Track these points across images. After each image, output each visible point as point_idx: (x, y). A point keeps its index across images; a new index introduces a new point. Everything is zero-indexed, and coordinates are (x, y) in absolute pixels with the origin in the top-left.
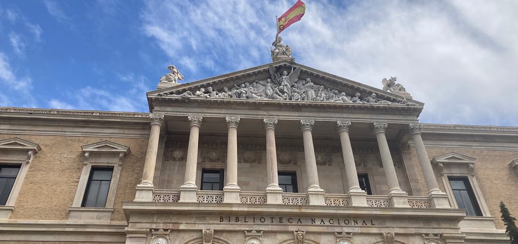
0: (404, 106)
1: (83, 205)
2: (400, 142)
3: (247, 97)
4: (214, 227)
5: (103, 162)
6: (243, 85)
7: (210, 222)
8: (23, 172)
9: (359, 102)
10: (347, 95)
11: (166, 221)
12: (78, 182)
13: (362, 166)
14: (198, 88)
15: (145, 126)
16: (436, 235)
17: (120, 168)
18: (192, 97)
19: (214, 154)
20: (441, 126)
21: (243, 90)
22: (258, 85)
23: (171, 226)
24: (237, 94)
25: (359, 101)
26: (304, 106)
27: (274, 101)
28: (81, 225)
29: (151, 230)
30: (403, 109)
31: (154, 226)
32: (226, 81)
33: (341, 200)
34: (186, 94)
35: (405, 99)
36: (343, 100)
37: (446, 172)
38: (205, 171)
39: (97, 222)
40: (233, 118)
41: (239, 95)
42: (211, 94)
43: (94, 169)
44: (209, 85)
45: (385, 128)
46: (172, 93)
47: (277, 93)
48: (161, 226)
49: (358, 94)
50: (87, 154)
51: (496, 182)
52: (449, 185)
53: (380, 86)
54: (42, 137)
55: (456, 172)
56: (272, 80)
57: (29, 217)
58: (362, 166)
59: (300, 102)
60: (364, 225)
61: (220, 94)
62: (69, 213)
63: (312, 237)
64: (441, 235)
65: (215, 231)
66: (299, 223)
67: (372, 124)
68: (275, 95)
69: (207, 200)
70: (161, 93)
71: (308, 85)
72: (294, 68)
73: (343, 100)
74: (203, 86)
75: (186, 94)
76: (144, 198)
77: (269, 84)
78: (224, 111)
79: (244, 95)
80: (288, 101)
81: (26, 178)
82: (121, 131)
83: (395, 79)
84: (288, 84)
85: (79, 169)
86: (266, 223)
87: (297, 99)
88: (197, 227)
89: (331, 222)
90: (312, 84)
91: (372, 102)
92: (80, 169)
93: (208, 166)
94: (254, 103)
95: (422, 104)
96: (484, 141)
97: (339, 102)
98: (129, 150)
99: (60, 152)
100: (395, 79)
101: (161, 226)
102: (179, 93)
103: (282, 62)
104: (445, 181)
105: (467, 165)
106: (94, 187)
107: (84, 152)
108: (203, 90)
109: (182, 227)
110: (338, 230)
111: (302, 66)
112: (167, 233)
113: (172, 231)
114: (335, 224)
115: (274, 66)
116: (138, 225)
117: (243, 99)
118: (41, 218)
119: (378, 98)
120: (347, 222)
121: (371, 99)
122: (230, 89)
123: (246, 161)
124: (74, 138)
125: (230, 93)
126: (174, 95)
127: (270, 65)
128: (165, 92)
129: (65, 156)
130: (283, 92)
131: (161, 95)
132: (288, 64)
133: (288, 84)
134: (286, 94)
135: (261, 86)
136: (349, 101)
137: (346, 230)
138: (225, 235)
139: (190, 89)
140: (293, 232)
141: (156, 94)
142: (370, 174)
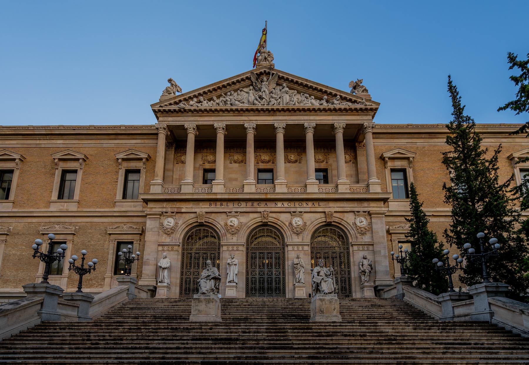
0: (363, 107)
1: (124, 196)
2: (354, 139)
3: (231, 104)
4: (205, 210)
5: (133, 165)
6: (229, 94)
7: (203, 207)
8: (80, 174)
9: (325, 105)
10: (316, 98)
11: (172, 206)
12: (117, 182)
13: (325, 162)
14: (191, 98)
15: (155, 135)
16: (365, 212)
17: (145, 170)
18: (187, 107)
19: (293, 156)
20: (389, 126)
21: (228, 98)
22: (242, 92)
23: (176, 210)
24: (223, 102)
25: (325, 104)
26: (278, 110)
27: (254, 107)
28: (123, 211)
29: (162, 213)
30: (361, 109)
31: (164, 210)
32: (214, 90)
33: (299, 188)
34: (181, 105)
35: (364, 100)
36: (311, 103)
37: (390, 164)
38: (260, 171)
39: (134, 209)
40: (220, 124)
41: (225, 102)
42: (203, 104)
43: (128, 172)
44: (200, 94)
45: (344, 128)
46: (170, 104)
47: (257, 99)
48: (169, 210)
49: (326, 97)
50: (120, 161)
51: (427, 172)
52: (389, 176)
53: (348, 90)
54: (87, 149)
55: (398, 164)
56: (254, 88)
57: (90, 207)
58: (325, 162)
59: (275, 107)
60: (313, 206)
61: (209, 103)
62: (114, 204)
63: (274, 215)
64: (369, 212)
65: (206, 213)
66: (266, 206)
67: (273, 125)
68: (256, 102)
69: (202, 191)
70: (162, 105)
71: (284, 90)
72: (273, 74)
73: (311, 103)
74: (195, 96)
75: (181, 105)
76: (156, 190)
77: (251, 91)
78: (213, 118)
79: (229, 103)
80: (265, 107)
81: (82, 180)
82: (143, 141)
83: (361, 81)
84: (266, 90)
85: (116, 172)
86: (242, 206)
87: (274, 104)
88: (193, 210)
89: (289, 204)
90: (287, 89)
91: (337, 104)
92: (117, 172)
93: (262, 166)
94: (237, 110)
95: (379, 104)
96: (429, 138)
97: (307, 105)
98: (149, 155)
99: (102, 160)
100: (361, 81)
101: (169, 210)
102: (176, 103)
103: (262, 68)
104: (388, 172)
105: (408, 158)
106: (130, 185)
107: (118, 159)
108: (195, 100)
109: (183, 210)
110: (293, 210)
111: (280, 71)
112: (174, 214)
113: (177, 213)
114: (292, 206)
115: (255, 73)
116: (154, 210)
117: (229, 107)
118: (97, 207)
119: (342, 100)
120: (300, 204)
121: (336, 102)
122: (218, 97)
123: (289, 162)
124: (110, 149)
125: (218, 101)
126: (173, 106)
127: (252, 72)
128: (165, 104)
129: (106, 162)
130: (261, 98)
131: (162, 107)
132: (267, 70)
133: (266, 90)
134: (264, 100)
135: (245, 94)
136: (316, 104)
137: (299, 210)
138: (213, 214)
139: (185, 100)
140: (261, 212)
141: (158, 106)
142: (329, 169)
